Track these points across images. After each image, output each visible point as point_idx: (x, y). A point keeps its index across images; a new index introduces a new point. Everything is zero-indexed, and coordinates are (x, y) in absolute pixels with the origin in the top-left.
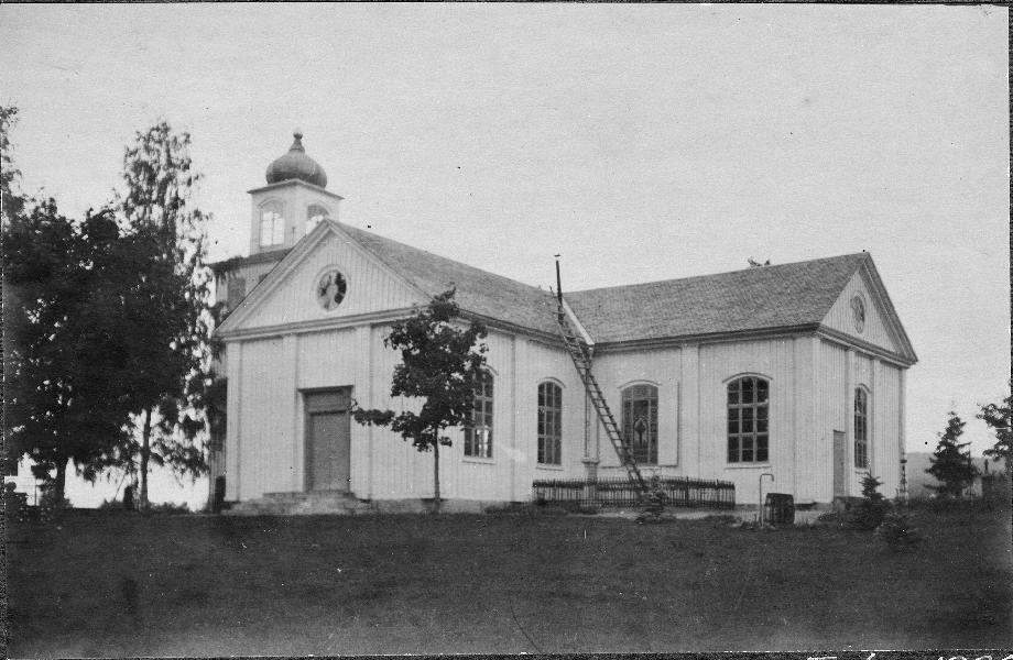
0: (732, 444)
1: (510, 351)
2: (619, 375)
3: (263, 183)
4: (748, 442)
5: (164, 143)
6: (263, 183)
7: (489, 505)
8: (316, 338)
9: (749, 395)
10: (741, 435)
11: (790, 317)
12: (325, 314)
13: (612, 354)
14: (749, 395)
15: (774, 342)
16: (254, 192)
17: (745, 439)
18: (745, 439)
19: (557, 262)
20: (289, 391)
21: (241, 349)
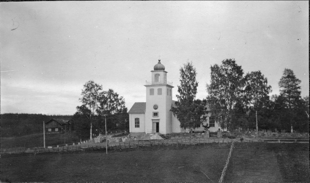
6: (153, 70)
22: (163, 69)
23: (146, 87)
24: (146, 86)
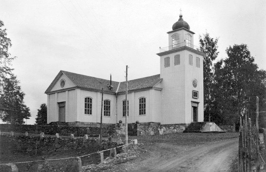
0: (85, 110)
1: (96, 95)
2: (122, 98)
3: (171, 30)
4: (88, 110)
5: (7, 51)
6: (171, 30)
7: (110, 124)
8: (61, 93)
9: (143, 101)
10: (141, 109)
11: (148, 85)
12: (61, 88)
13: (122, 94)
14: (143, 101)
15: (141, 92)
16: (168, 33)
17: (90, 110)
18: (90, 110)
19: (111, 76)
20: (56, 102)
21: (68, 92)
22: (186, 27)
23: (159, 57)
24: (159, 54)
